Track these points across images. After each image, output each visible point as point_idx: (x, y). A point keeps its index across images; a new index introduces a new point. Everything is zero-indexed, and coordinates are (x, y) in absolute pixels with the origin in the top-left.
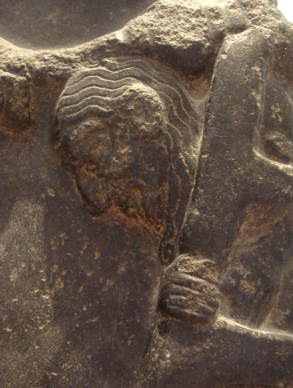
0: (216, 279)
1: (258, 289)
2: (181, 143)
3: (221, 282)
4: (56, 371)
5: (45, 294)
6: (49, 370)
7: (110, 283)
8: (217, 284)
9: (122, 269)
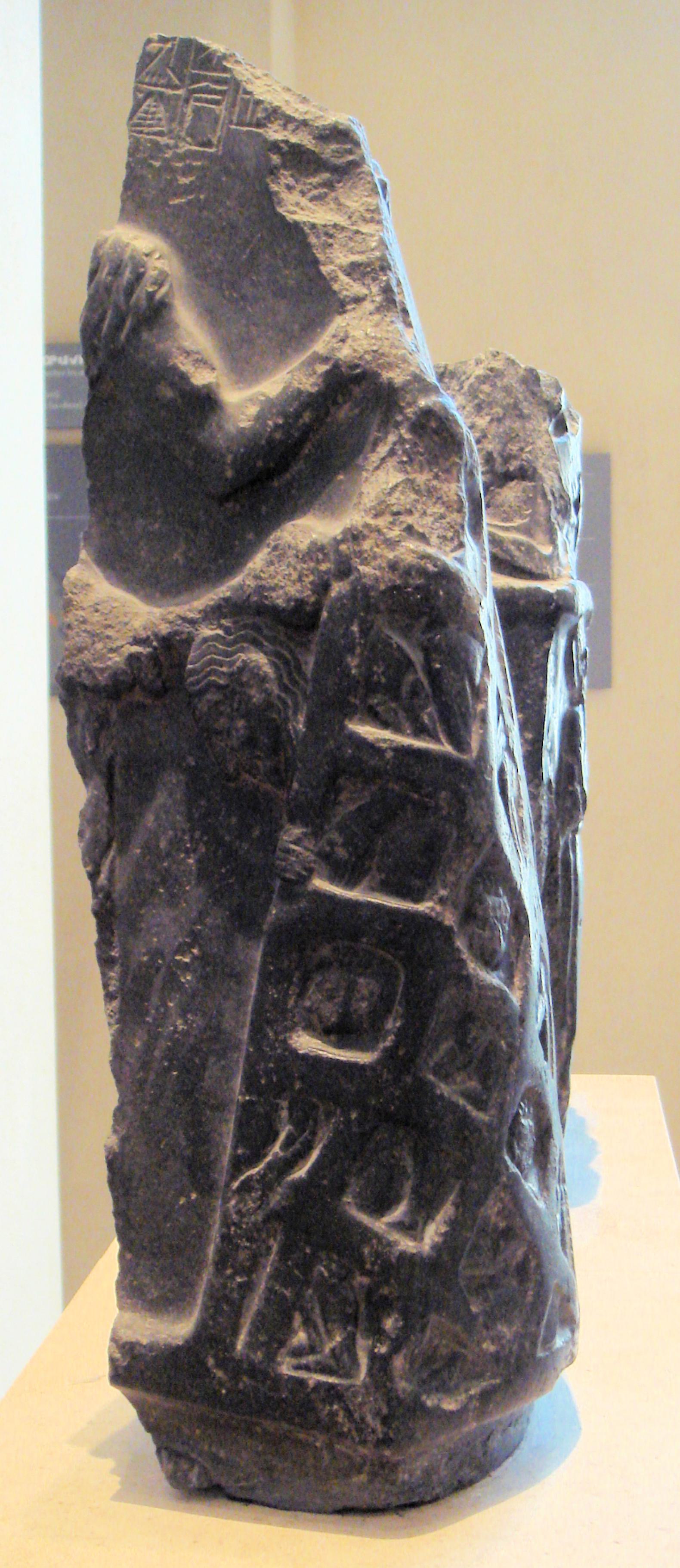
0: (311, 847)
1: (350, 854)
2: (290, 713)
3: (316, 850)
4: (201, 925)
5: (189, 858)
6: (194, 924)
7: (245, 846)
8: (312, 851)
9: (256, 833)
